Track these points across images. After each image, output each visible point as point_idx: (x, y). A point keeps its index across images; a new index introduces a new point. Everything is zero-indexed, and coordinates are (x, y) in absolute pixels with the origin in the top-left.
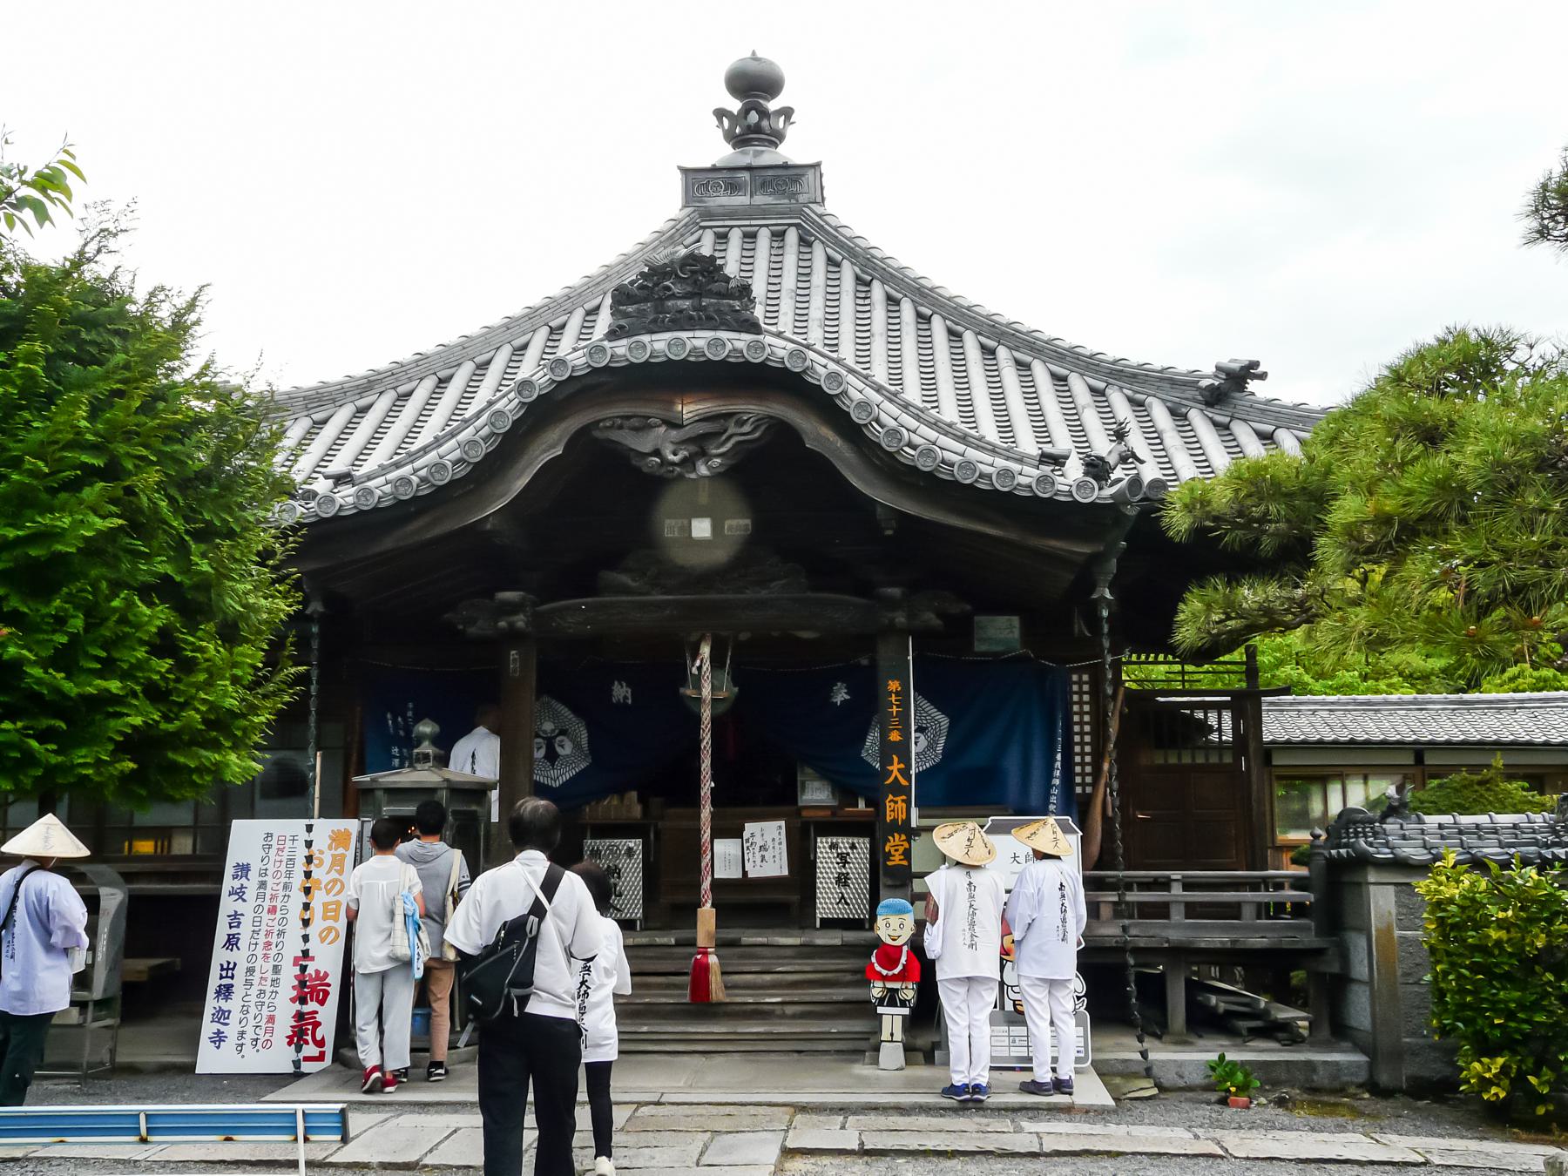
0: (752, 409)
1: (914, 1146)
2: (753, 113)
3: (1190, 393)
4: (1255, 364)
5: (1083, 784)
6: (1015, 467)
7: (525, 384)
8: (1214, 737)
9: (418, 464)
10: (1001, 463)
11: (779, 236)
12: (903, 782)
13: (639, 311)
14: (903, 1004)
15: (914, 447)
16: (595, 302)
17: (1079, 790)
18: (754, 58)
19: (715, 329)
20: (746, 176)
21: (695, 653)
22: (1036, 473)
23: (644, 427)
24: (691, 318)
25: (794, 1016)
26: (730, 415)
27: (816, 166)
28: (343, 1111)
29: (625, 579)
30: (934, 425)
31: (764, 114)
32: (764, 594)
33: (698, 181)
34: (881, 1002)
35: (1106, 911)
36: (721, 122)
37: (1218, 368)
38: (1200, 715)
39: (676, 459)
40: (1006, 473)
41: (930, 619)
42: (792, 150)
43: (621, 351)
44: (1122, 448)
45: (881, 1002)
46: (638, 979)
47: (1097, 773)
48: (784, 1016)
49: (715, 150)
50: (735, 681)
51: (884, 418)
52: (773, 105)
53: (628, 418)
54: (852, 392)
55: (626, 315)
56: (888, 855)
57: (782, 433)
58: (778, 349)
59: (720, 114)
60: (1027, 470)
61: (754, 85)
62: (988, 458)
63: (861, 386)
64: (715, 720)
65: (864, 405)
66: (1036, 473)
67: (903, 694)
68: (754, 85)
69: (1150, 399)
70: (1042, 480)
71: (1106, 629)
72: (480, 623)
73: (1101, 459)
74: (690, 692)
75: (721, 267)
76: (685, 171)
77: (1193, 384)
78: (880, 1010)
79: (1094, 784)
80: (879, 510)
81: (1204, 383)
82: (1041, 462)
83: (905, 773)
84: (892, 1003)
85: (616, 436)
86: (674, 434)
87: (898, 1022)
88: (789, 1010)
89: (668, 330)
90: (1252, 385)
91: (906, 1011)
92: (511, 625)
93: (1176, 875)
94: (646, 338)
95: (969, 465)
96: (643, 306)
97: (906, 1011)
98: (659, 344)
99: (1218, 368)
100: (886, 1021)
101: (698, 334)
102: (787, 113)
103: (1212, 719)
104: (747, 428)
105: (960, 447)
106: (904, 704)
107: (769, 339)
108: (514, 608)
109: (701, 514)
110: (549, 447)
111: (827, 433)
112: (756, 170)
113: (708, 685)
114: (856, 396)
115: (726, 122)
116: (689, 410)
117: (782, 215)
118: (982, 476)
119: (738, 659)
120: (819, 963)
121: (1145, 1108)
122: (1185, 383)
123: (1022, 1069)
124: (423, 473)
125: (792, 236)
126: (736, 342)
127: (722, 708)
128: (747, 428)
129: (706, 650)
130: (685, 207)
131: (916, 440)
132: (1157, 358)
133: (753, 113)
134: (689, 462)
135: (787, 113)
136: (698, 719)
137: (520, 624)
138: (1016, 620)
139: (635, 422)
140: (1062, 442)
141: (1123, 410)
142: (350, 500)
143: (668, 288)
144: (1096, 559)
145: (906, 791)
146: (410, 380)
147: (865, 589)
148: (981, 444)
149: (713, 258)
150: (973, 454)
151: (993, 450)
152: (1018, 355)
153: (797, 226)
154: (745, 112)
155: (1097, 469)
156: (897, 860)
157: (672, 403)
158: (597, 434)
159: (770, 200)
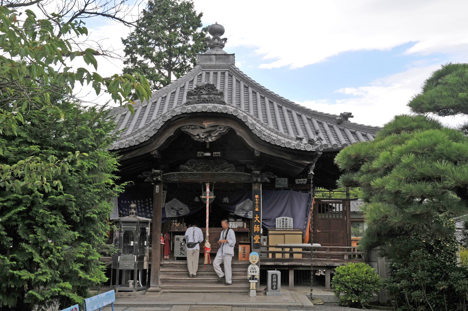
0: (223, 124)
2: (216, 39)
4: (351, 114)
6: (290, 141)
7: (164, 116)
8: (334, 210)
9: (135, 136)
10: (287, 140)
11: (223, 73)
12: (259, 222)
13: (194, 98)
14: (256, 279)
15: (265, 136)
16: (174, 90)
18: (216, 24)
19: (214, 103)
22: (296, 143)
24: (207, 100)
26: (217, 126)
27: (234, 55)
29: (187, 167)
31: (219, 39)
32: (223, 172)
38: (331, 204)
40: (289, 143)
41: (267, 180)
42: (227, 49)
43: (189, 108)
44: (318, 137)
46: (117, 282)
50: (215, 195)
51: (257, 128)
52: (222, 37)
54: (249, 121)
56: (254, 241)
57: (231, 131)
58: (230, 109)
60: (293, 142)
62: (283, 139)
63: (251, 119)
65: (253, 124)
66: (296, 143)
67: (259, 198)
69: (323, 122)
70: (298, 145)
71: (312, 182)
72: (148, 178)
73: (313, 139)
75: (216, 87)
78: (250, 281)
80: (255, 151)
81: (338, 118)
82: (297, 140)
83: (259, 219)
84: (253, 279)
85: (187, 130)
86: (203, 130)
87: (255, 284)
89: (201, 103)
90: (350, 119)
91: (257, 281)
92: (157, 179)
94: (196, 105)
95: (279, 140)
96: (195, 97)
97: (257, 281)
98: (200, 107)
101: (209, 104)
102: (225, 39)
103: (334, 205)
104: (222, 129)
105: (276, 136)
106: (259, 201)
107: (228, 106)
108: (158, 174)
110: (171, 133)
117: (224, 68)
118: (282, 143)
119: (216, 189)
122: (332, 118)
124: (136, 139)
125: (227, 74)
126: (219, 108)
127: (212, 201)
128: (222, 129)
131: (266, 134)
133: (216, 39)
135: (225, 39)
137: (159, 179)
138: (286, 179)
139: (192, 127)
140: (301, 135)
141: (317, 126)
142: (117, 145)
143: (202, 92)
144: (310, 165)
145: (259, 224)
146: (125, 111)
147: (250, 171)
148: (281, 135)
149: (214, 85)
150: (280, 137)
151: (284, 136)
153: (228, 71)
154: (214, 39)
155: (311, 142)
156: (257, 242)
157: (203, 122)
158: (182, 130)
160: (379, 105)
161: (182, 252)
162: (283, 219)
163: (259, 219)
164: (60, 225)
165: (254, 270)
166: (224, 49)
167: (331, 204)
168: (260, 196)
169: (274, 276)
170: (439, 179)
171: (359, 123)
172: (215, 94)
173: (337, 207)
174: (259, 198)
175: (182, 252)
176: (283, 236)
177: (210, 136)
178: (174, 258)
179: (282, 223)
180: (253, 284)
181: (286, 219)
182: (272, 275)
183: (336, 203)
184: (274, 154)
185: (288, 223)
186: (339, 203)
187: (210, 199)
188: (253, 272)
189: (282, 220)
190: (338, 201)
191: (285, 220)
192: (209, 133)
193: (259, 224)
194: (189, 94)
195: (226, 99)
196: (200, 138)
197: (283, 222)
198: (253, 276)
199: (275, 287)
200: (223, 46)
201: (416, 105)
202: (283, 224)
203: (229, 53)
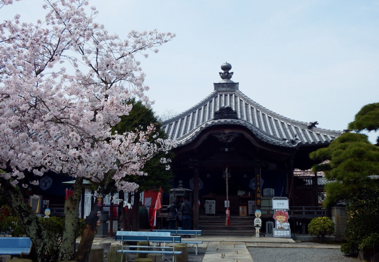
1: (266, 246)
3: (305, 127)
4: (317, 122)
5: (287, 192)
8: (307, 184)
9: (183, 140)
11: (231, 95)
14: (259, 227)
17: (286, 193)
20: (226, 84)
21: (225, 170)
22: (283, 142)
23: (220, 134)
25: (241, 230)
26: (233, 133)
30: (261, 131)
31: (228, 73)
33: (217, 85)
34: (256, 226)
35: (292, 213)
36: (220, 75)
38: (304, 180)
39: (225, 139)
42: (234, 79)
45: (256, 226)
47: (289, 190)
53: (217, 133)
55: (216, 116)
57: (242, 136)
59: (220, 73)
60: (281, 142)
61: (227, 68)
62: (275, 140)
64: (228, 180)
65: (255, 131)
67: (259, 177)
68: (227, 68)
74: (224, 176)
76: (215, 84)
77: (306, 125)
79: (289, 192)
84: (258, 227)
86: (225, 136)
88: (240, 228)
90: (316, 125)
91: (260, 228)
93: (304, 207)
97: (260, 228)
102: (232, 73)
104: (236, 135)
106: (260, 179)
107: (240, 121)
110: (205, 137)
111: (249, 135)
112: (227, 84)
113: (227, 175)
116: (227, 131)
120: (244, 221)
121: (300, 243)
123: (309, 209)
128: (236, 135)
129: (227, 169)
134: (227, 140)
135: (232, 73)
140: (285, 137)
150: (268, 137)
152: (275, 119)
154: (225, 73)
155: (293, 142)
156: (259, 204)
159: (230, 89)
161: (211, 210)
162: (268, 190)
163: (260, 190)
166: (231, 79)
167: (304, 180)
168: (260, 175)
169: (270, 225)
171: (323, 128)
172: (232, 113)
173: (309, 182)
175: (211, 210)
177: (229, 139)
180: (258, 230)
181: (270, 190)
182: (269, 224)
183: (308, 179)
185: (271, 192)
186: (310, 179)
187: (228, 178)
189: (267, 191)
190: (309, 178)
191: (269, 191)
192: (229, 137)
193: (260, 193)
194: (216, 113)
195: (239, 117)
196: (223, 140)
197: (268, 191)
198: (258, 225)
199: (270, 232)
200: (231, 77)
201: (352, 126)
202: (268, 193)
203: (235, 82)
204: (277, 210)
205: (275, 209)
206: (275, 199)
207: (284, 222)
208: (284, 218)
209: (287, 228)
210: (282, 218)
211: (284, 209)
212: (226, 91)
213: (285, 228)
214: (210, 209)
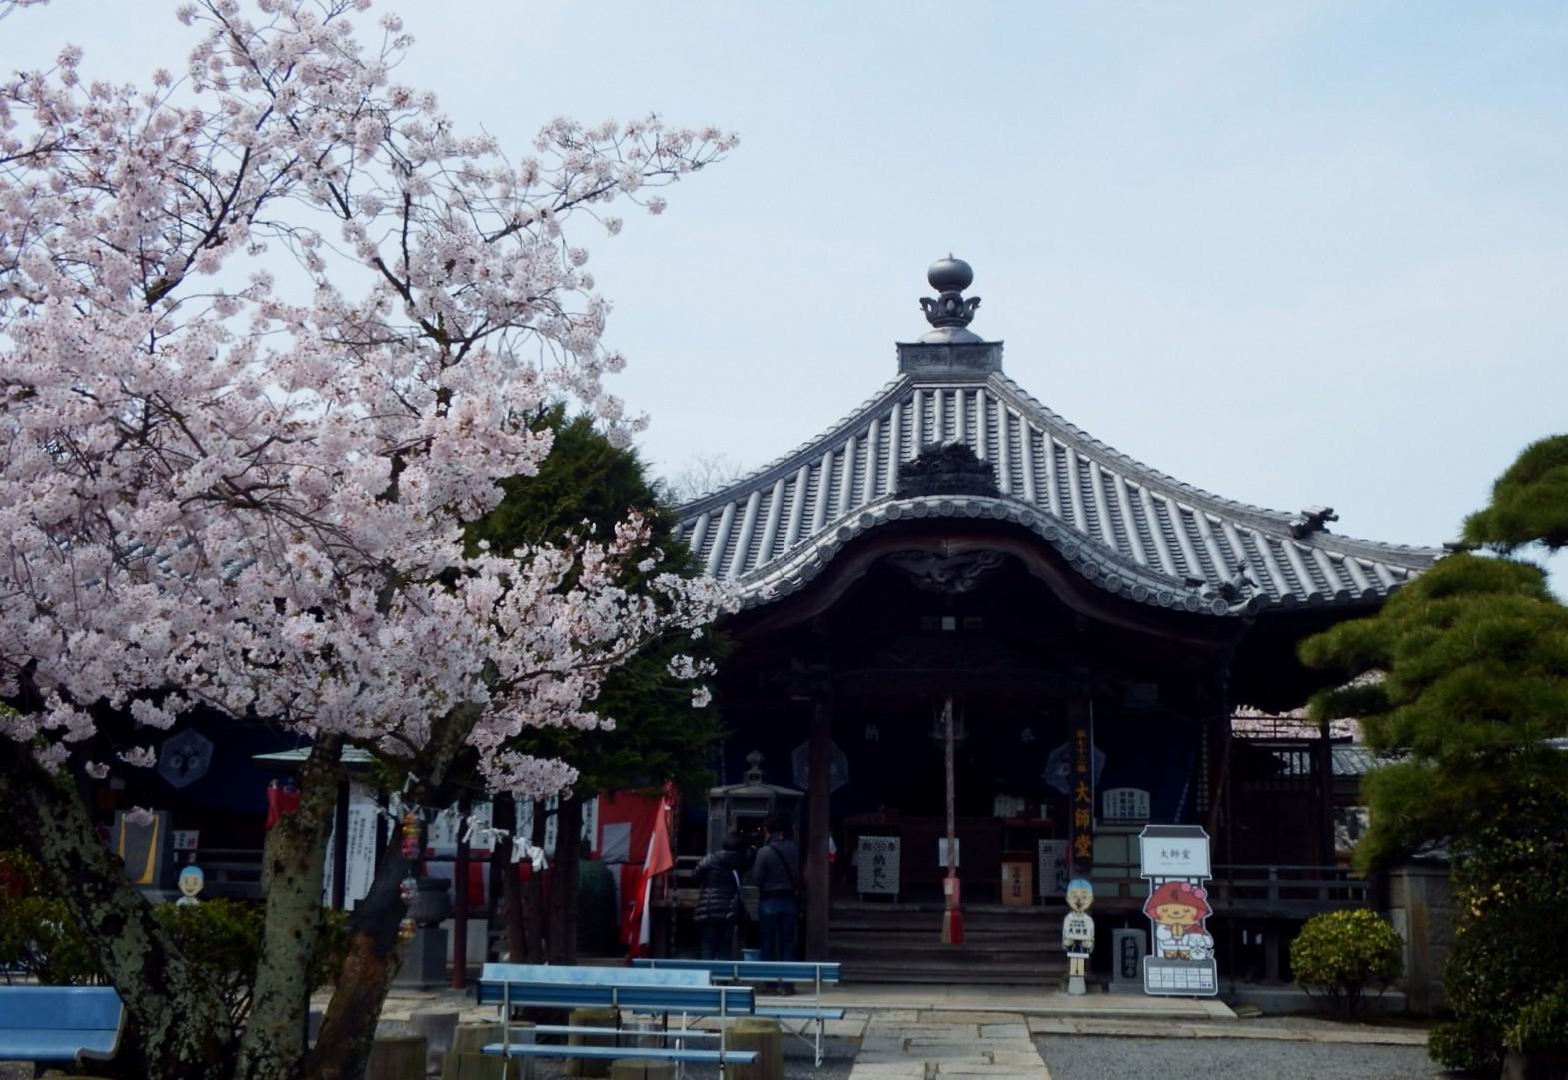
3: (1283, 529)
4: (1331, 510)
8: (1287, 772)
9: (767, 580)
10: (1161, 587)
11: (970, 395)
12: (1088, 800)
14: (1085, 951)
21: (942, 708)
23: (921, 557)
28: (751, 994)
30: (1095, 546)
31: (959, 302)
33: (910, 353)
34: (1070, 949)
35: (1224, 893)
36: (925, 308)
37: (1304, 512)
38: (1277, 754)
42: (981, 327)
45: (1070, 949)
47: (1212, 797)
48: (1000, 961)
49: (925, 331)
53: (910, 552)
57: (1014, 565)
59: (925, 301)
60: (1179, 592)
61: (952, 280)
64: (956, 753)
65: (1071, 548)
67: (1087, 740)
68: (952, 280)
74: (938, 736)
76: (902, 346)
77: (1286, 522)
81: (1294, 523)
87: (1082, 964)
90: (1328, 524)
93: (1273, 869)
97: (1087, 956)
99: (1304, 512)
100: (1073, 963)
102: (976, 301)
105: (1133, 576)
106: (1088, 747)
109: (949, 615)
110: (858, 568)
112: (952, 347)
113: (950, 732)
114: (1045, 526)
115: (930, 307)
116: (952, 547)
123: (1297, 875)
128: (991, 561)
129: (949, 706)
130: (900, 372)
132: (1261, 502)
134: (951, 583)
135: (976, 301)
136: (944, 754)
140: (1196, 572)
148: (1134, 568)
152: (1155, 494)
154: (944, 300)
155: (1230, 594)
156: (1083, 853)
159: (964, 368)
160: (1408, 494)
162: (1123, 794)
163: (1089, 794)
164: (315, 801)
165: (1080, 927)
166: (972, 327)
167: (1277, 754)
169: (1129, 943)
170: (1504, 718)
171: (1356, 534)
172: (972, 471)
173: (1296, 762)
174: (1087, 740)
175: (879, 880)
176: (1123, 840)
178: (858, 894)
179: (1119, 805)
181: (1132, 795)
182: (1124, 940)
183: (1291, 751)
184: (1131, 626)
185: (1137, 805)
186: (1302, 751)
188: (1079, 931)
189: (1119, 798)
190: (1295, 745)
191: (1127, 797)
192: (958, 571)
193: (1088, 806)
194: (905, 470)
195: (1004, 486)
197: (1123, 801)
199: (1130, 971)
200: (969, 318)
202: (1123, 808)
203: (988, 338)
204: (1159, 881)
205: (1154, 877)
206: (1152, 834)
207: (1188, 930)
208: (1188, 914)
209: (1202, 956)
210: (1182, 913)
211: (1189, 878)
212: (950, 378)
213: (1194, 956)
214: (878, 872)
